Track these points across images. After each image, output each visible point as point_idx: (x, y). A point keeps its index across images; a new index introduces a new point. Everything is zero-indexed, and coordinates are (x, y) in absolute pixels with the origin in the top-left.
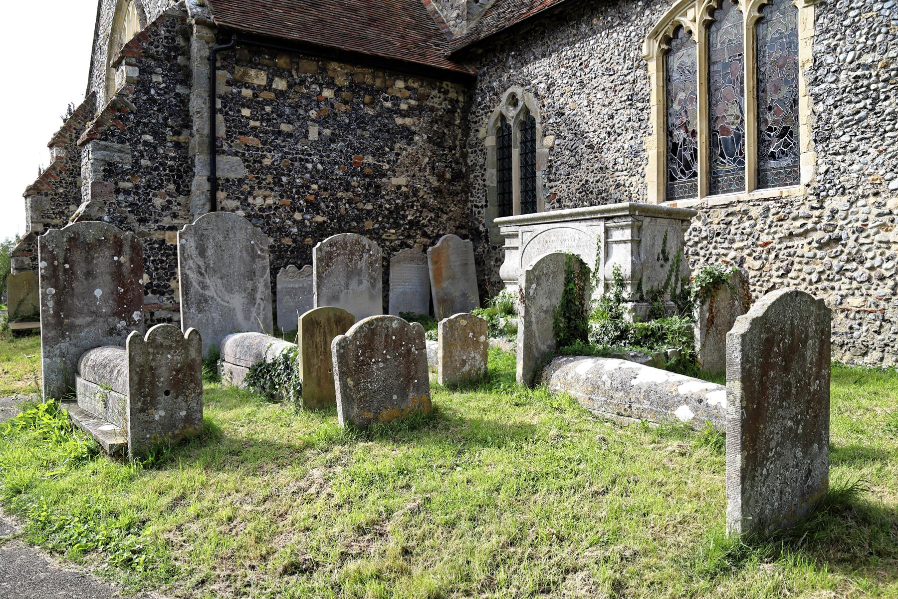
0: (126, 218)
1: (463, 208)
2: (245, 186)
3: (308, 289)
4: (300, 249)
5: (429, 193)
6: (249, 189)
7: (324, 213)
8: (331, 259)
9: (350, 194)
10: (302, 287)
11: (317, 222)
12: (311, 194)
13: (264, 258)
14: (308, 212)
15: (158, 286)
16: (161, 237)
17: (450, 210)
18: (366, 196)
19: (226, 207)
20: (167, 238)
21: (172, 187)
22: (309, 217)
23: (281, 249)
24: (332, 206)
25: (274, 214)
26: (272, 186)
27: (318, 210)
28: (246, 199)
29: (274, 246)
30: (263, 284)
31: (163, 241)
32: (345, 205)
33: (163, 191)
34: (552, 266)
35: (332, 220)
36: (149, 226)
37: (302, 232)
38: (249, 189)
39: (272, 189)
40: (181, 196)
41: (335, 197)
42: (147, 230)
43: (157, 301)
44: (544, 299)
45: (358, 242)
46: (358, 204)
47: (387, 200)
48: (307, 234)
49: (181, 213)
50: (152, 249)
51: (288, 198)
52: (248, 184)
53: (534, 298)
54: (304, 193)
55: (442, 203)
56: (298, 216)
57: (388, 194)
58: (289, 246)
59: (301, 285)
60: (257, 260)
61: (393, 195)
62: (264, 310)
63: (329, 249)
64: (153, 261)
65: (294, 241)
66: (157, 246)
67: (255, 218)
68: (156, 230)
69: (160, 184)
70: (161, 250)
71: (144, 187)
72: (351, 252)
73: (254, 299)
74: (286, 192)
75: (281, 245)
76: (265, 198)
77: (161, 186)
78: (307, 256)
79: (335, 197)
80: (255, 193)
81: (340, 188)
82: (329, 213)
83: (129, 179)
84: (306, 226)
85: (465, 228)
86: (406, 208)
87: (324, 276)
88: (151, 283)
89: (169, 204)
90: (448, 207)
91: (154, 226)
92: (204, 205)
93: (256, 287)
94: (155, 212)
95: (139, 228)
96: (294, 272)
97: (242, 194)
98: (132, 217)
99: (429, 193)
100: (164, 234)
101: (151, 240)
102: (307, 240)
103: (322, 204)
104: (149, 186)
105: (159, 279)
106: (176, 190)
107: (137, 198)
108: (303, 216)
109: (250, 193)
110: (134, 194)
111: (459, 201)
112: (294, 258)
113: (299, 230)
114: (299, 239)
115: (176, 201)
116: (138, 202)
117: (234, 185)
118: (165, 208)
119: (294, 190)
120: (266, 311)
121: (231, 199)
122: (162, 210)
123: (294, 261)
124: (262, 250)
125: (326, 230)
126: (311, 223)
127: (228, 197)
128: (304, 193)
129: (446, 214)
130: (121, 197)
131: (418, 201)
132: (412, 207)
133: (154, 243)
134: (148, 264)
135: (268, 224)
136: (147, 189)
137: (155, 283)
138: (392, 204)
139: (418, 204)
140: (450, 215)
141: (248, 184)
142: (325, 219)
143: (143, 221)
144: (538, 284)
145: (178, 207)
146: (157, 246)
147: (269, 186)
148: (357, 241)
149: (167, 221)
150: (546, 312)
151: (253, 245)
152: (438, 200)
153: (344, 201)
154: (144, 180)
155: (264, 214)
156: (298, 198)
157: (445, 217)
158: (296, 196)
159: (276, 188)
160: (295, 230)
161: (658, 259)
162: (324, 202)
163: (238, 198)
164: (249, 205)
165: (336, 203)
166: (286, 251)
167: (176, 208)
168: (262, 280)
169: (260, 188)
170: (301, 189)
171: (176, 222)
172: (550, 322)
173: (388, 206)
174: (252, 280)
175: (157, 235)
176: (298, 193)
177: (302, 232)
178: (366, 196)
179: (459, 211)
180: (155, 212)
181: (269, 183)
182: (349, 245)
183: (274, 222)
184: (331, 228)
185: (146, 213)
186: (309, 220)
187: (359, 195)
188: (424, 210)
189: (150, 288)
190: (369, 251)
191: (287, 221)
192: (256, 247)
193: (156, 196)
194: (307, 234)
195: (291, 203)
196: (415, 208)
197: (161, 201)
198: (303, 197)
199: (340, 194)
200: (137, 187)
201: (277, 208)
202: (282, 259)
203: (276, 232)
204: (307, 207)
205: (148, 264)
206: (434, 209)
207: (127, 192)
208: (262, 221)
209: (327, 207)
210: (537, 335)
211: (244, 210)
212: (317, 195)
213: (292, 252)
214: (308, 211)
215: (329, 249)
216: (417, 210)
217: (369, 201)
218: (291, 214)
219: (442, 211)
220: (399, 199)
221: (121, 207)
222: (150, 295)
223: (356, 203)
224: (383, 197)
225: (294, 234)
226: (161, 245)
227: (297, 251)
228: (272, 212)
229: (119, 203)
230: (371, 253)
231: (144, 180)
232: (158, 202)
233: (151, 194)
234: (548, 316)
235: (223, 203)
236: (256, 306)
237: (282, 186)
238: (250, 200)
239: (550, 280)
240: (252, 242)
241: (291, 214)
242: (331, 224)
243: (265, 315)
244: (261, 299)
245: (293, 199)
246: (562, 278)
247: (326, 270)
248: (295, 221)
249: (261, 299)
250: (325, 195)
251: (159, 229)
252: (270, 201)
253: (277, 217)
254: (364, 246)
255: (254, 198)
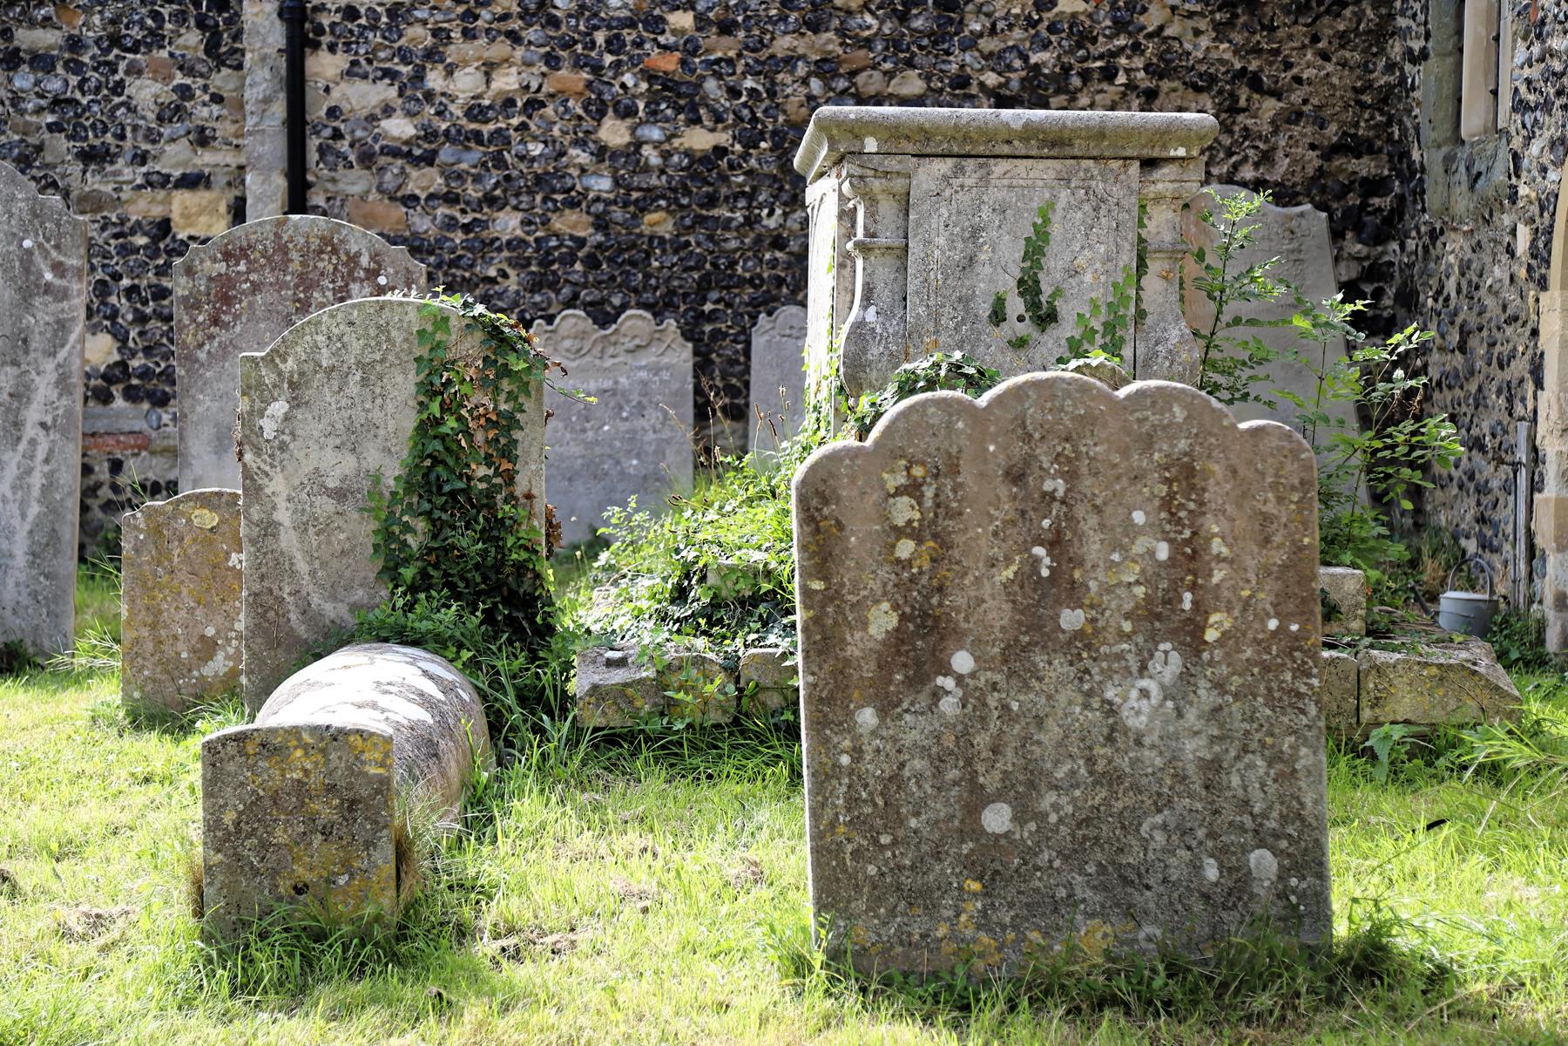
0: (39, 148)
1: (1366, 68)
2: (418, 31)
3: (635, 398)
4: (621, 251)
5: (1191, 15)
6: (429, 41)
7: (718, 118)
8: (227, 300)
9: (828, 41)
10: (614, 392)
11: (688, 153)
12: (665, 48)
13: (63, 295)
14: (653, 115)
15: (145, 374)
16: (157, 212)
17: (1298, 80)
18: (894, 43)
19: (345, 107)
20: (176, 217)
21: (192, 39)
22: (655, 133)
23: (549, 252)
24: (753, 92)
25: (523, 127)
26: (516, 25)
27: (694, 108)
28: (419, 76)
29: (523, 243)
30: (52, 377)
31: (164, 226)
32: (805, 82)
33: (164, 54)
34: (356, 346)
35: (750, 143)
36: (117, 173)
37: (629, 189)
38: (429, 41)
39: (515, 38)
40: (225, 71)
41: (764, 54)
42: (108, 188)
43: (140, 425)
44: (329, 452)
45: (329, 245)
46: (861, 79)
47: (988, 56)
48: (650, 195)
49: (225, 129)
50: (126, 250)
51: (578, 65)
52: (425, 22)
53: (283, 447)
54: (639, 44)
55: (1257, 51)
56: (614, 132)
57: (993, 31)
58: (581, 242)
59: (608, 384)
60: (37, 301)
61: (1018, 33)
62: (47, 461)
63: (221, 267)
64: (131, 291)
65: (601, 223)
66: (141, 241)
67: (454, 142)
68: (140, 187)
69: (152, 32)
70: (155, 254)
71: (98, 42)
72: (302, 277)
73: (18, 425)
74: (568, 45)
75: (546, 239)
76: (489, 69)
77: (156, 39)
78: (647, 276)
79: (764, 54)
80: (452, 53)
81: (784, 19)
82: (739, 118)
83: (47, 19)
84: (647, 169)
85: (1372, 151)
86: (1076, 82)
87: (202, 355)
88: (123, 365)
89: (183, 98)
90: (1288, 66)
91: (131, 173)
92: (267, 101)
93: (27, 387)
94: (135, 128)
95: (84, 181)
96: (582, 336)
97: (405, 61)
98: (61, 145)
99: (1191, 15)
100: (167, 202)
101: (123, 221)
102: (650, 217)
103: (711, 85)
104: (115, 40)
105: (148, 351)
106: (207, 51)
107: (74, 80)
108: (633, 130)
109: (432, 55)
110: (66, 65)
111: (1342, 36)
112: (598, 284)
113: (617, 182)
114: (618, 214)
115: (205, 88)
116: (78, 95)
117: (374, 28)
118: (171, 112)
119: (600, 37)
120: (53, 464)
121: (365, 77)
122: (160, 119)
123: (595, 295)
124: (58, 268)
125: (724, 179)
126: (666, 155)
127: (352, 72)
128: (639, 44)
129: (1277, 94)
130: (23, 79)
131: (1137, 48)
132: (1109, 74)
133: (133, 232)
134: (113, 300)
135: (499, 162)
136: (107, 51)
137: (135, 363)
138: (1009, 68)
139: (1138, 62)
140: (1296, 97)
141: (425, 22)
142: (723, 138)
143: (93, 157)
144: (296, 403)
145: (216, 109)
146: (141, 241)
147: (503, 26)
148: (326, 240)
149: (175, 157)
150: (340, 494)
151: (29, 252)
152: (1238, 38)
153: (801, 69)
154: (96, 19)
155: (487, 129)
156: (617, 65)
157: (1270, 106)
158: (608, 59)
159: (532, 34)
160: (602, 184)
161: (998, 316)
162: (718, 76)
163: (390, 74)
164: (429, 96)
165: (770, 78)
166: (569, 260)
167: (205, 112)
168: (49, 365)
169: (468, 35)
170: (629, 36)
171: (205, 159)
172: (361, 530)
173: (991, 79)
174: (15, 363)
175: (142, 204)
176: (614, 45)
177: (629, 189)
178: (894, 43)
179: (1342, 80)
180: (135, 128)
181: (505, 17)
182: (294, 255)
183: (522, 158)
184: (750, 173)
185: (105, 130)
186: (657, 145)
187: (868, 43)
188: (1166, 85)
189: (118, 381)
190: (372, 274)
191: (573, 152)
192: (37, 257)
193: (139, 73)
194: (650, 195)
195: (589, 85)
196: (1121, 79)
197: (156, 87)
198: (634, 62)
199: (783, 44)
200: (75, 44)
201: (533, 105)
202: (554, 286)
203: (530, 192)
204: (652, 100)
205: (113, 300)
206: (1212, 79)
207: (42, 62)
208: (477, 153)
209: (734, 93)
210: (302, 566)
211: (410, 114)
212: (691, 48)
213: (592, 263)
214: (655, 113)
215: (221, 267)
216: (1131, 86)
217: (910, 64)
218: (589, 123)
219: (1255, 84)
220: (1046, 46)
221: (22, 112)
222: (119, 403)
223: (853, 74)
224: (970, 44)
225: (597, 199)
226: (155, 240)
227: (610, 260)
228: (515, 121)
229: (16, 100)
230: (382, 280)
231: (96, 19)
232: (146, 92)
233: (122, 66)
234: (349, 507)
235: (336, 94)
236: (22, 446)
237: (554, 22)
238: (434, 79)
239: (353, 388)
240: (27, 243)
241: (589, 123)
242: (745, 156)
243: (50, 476)
244: (43, 425)
245: (597, 69)
246: (404, 385)
247: (211, 337)
248: (601, 152)
249: (43, 425)
250: (723, 47)
251: (150, 184)
252: (507, 81)
253: (535, 138)
254: (353, 259)
255: (450, 71)
